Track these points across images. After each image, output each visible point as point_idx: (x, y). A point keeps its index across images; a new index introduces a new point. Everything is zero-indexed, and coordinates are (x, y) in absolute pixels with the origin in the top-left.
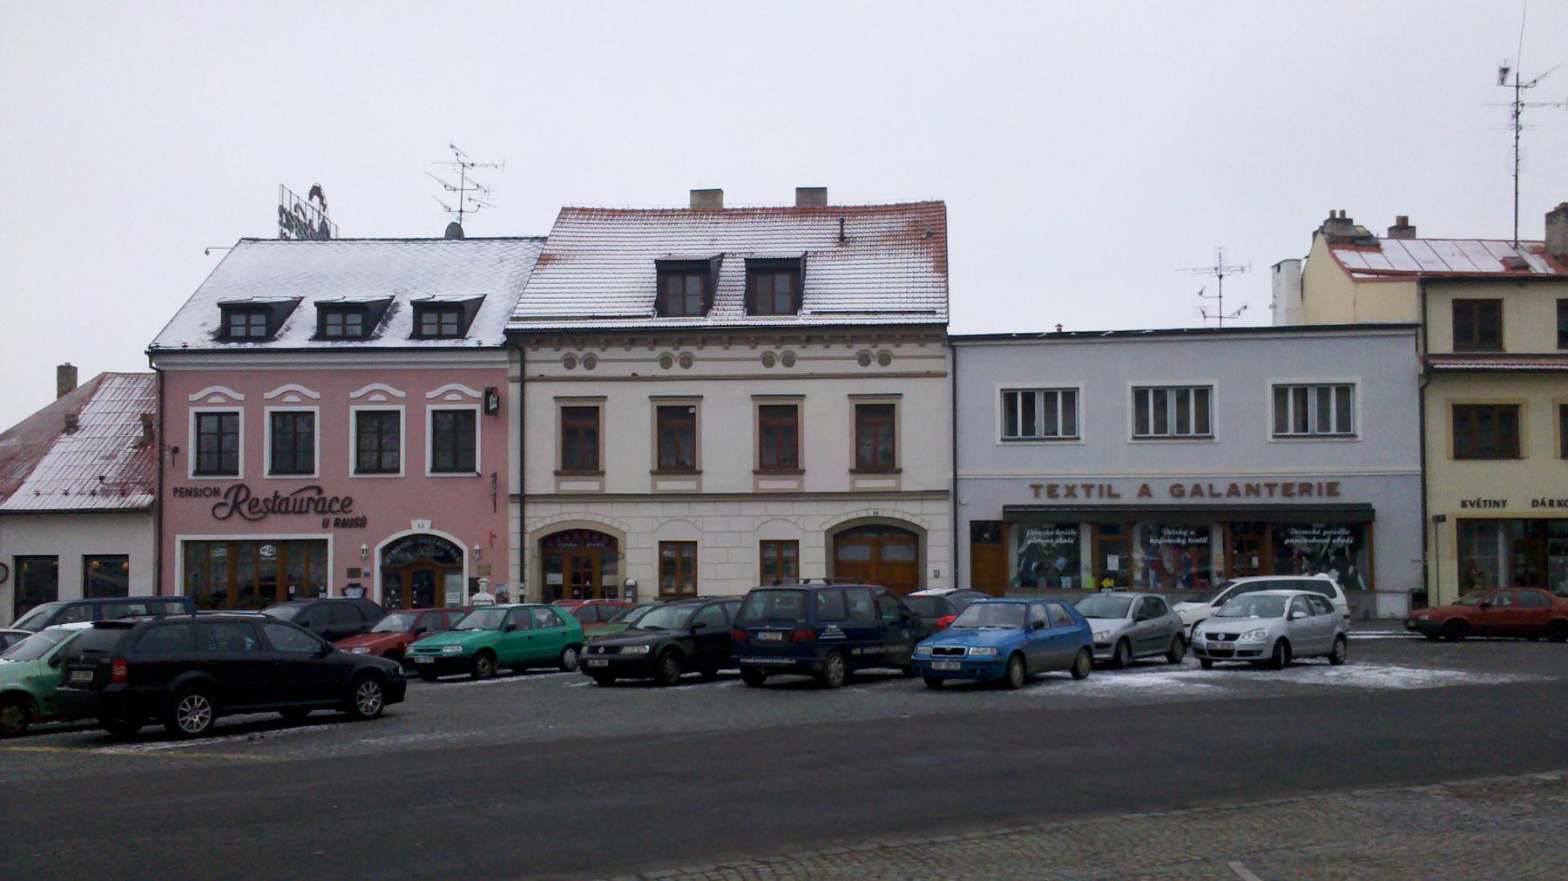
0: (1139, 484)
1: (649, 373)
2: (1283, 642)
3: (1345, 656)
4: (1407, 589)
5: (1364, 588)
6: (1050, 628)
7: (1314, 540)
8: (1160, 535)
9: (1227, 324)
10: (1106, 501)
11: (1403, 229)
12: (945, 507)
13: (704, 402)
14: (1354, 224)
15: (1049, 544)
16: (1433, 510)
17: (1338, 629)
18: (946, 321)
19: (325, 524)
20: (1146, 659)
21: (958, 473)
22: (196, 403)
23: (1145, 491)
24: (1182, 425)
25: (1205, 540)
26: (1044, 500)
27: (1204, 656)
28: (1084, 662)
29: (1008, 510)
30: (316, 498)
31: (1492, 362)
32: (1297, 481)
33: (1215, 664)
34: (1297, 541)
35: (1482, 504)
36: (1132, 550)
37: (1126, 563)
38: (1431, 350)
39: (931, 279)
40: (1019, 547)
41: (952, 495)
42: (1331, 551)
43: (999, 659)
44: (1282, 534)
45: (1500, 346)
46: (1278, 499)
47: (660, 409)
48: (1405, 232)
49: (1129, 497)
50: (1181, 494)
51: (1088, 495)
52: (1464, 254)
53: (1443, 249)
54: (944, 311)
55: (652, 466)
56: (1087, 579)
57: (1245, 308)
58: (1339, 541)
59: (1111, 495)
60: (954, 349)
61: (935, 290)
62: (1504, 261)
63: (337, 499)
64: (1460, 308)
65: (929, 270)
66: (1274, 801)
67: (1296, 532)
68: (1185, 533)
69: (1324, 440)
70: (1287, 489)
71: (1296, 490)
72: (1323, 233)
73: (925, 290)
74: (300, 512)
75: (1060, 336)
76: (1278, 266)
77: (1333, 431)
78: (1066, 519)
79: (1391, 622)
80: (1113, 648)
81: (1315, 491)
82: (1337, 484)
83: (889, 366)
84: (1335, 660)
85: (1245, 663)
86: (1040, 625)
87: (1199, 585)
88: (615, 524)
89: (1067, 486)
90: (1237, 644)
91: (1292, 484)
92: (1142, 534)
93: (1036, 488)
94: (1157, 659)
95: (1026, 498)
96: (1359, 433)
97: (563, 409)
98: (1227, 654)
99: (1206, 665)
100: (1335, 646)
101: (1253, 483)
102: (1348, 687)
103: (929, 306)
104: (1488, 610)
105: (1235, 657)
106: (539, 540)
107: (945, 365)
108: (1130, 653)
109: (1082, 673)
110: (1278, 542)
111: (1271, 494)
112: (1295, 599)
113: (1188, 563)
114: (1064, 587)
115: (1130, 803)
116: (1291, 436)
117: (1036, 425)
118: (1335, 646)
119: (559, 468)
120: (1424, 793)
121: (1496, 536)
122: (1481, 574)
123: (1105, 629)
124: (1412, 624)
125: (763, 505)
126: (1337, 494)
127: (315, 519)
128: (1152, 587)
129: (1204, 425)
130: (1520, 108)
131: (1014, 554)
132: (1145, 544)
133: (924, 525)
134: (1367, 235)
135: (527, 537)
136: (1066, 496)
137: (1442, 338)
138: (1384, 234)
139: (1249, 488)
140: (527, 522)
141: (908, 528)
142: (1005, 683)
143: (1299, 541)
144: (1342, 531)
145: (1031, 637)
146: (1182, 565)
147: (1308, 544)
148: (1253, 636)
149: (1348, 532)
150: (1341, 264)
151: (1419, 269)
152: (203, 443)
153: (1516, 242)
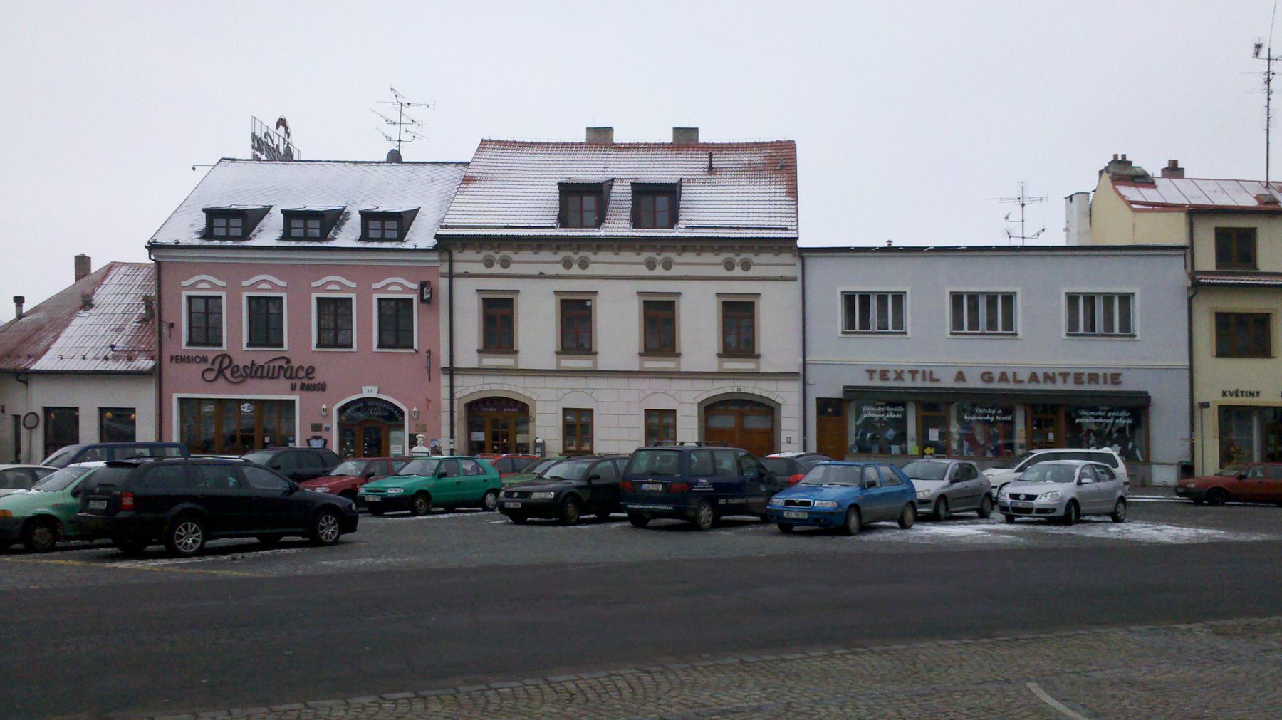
0: (955, 371)
1: (553, 272)
2: (1073, 502)
3: (1125, 515)
5: (1141, 460)
6: (881, 486)
7: (1100, 420)
8: (972, 413)
9: (1028, 243)
10: (928, 384)
11: (1173, 170)
12: (796, 386)
14: (1134, 165)
15: (881, 419)
16: (1200, 397)
17: (1119, 493)
18: (796, 236)
20: (961, 514)
21: (807, 359)
22: (378, 291)
23: (960, 376)
24: (992, 324)
25: (1008, 418)
26: (877, 382)
28: (909, 515)
29: (847, 390)
31: (1247, 278)
33: (1017, 519)
34: (1086, 420)
35: (1240, 394)
36: (949, 425)
37: (944, 435)
40: (856, 420)
41: (802, 376)
42: (1114, 430)
43: (840, 510)
44: (1073, 415)
45: (1254, 266)
46: (1071, 386)
48: (1176, 172)
49: (947, 382)
50: (991, 380)
51: (913, 379)
52: (1224, 191)
53: (1208, 187)
54: (794, 228)
56: (912, 447)
57: (1043, 230)
58: (1121, 421)
59: (933, 380)
60: (803, 258)
61: (787, 211)
62: (1257, 198)
63: (301, 368)
64: (1222, 235)
65: (782, 195)
66: (1065, 633)
67: (1085, 413)
68: (994, 412)
70: (1078, 378)
71: (1085, 378)
72: (1108, 172)
74: (273, 378)
75: (890, 250)
76: (1071, 198)
77: (1117, 331)
78: (895, 398)
79: (1164, 488)
80: (933, 504)
81: (1101, 380)
82: (1119, 375)
84: (1116, 519)
85: (1042, 519)
86: (872, 484)
87: (1005, 454)
88: (527, 394)
89: (896, 371)
90: (1036, 503)
91: (1083, 374)
92: (958, 412)
93: (871, 372)
94: (970, 514)
95: (862, 380)
96: (1138, 333)
98: (1028, 511)
99: (1010, 520)
101: (1050, 372)
104: (1244, 480)
105: (1034, 514)
107: (796, 271)
108: (947, 509)
109: (908, 524)
110: (1070, 421)
111: (1065, 381)
112: (1084, 467)
113: (996, 437)
114: (893, 453)
115: (946, 631)
120: (1189, 630)
121: (1251, 420)
122: (1238, 452)
123: (926, 488)
124: (1181, 490)
127: (284, 383)
130: (1271, 77)
131: (852, 425)
132: (960, 420)
134: (1144, 174)
135: (456, 402)
136: (896, 379)
137: (1206, 259)
138: (1159, 174)
140: (455, 390)
142: (844, 531)
144: (1124, 413)
146: (991, 438)
148: (1048, 497)
150: (1123, 197)
152: (193, 319)
153: (1268, 182)
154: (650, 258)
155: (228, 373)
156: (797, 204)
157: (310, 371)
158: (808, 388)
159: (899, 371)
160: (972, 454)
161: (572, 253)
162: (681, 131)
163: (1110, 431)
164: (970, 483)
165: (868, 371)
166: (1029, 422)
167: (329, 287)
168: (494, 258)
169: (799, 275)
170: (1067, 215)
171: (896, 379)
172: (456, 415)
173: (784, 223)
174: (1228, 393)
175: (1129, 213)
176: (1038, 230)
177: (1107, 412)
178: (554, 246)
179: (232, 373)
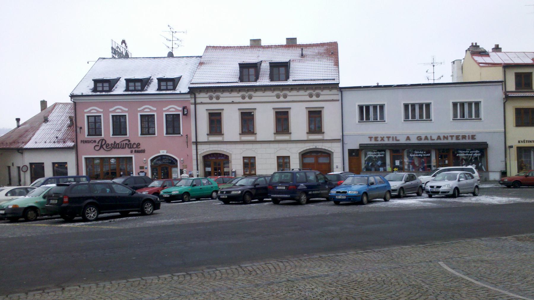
1: (238, 101)
2: (456, 188)
4: (500, 171)
5: (484, 170)
7: (467, 154)
8: (413, 153)
9: (436, 82)
10: (395, 142)
11: (497, 49)
12: (339, 145)
13: (257, 111)
14: (480, 47)
15: (375, 157)
16: (508, 144)
17: (476, 184)
18: (338, 82)
19: (132, 152)
20: (409, 195)
22: (165, 111)
23: (408, 138)
24: (421, 116)
25: (429, 155)
26: (373, 142)
27: (429, 194)
28: (388, 196)
29: (361, 145)
30: (128, 143)
32: (461, 135)
33: (433, 196)
34: (461, 155)
35: (525, 142)
37: (402, 163)
38: (508, 89)
39: (333, 68)
40: (365, 158)
41: (342, 140)
42: (473, 158)
43: (359, 195)
44: (456, 153)
46: (454, 141)
49: (403, 140)
50: (421, 139)
51: (388, 140)
52: (518, 57)
53: (510, 55)
56: (389, 168)
57: (442, 76)
58: (476, 155)
59: (396, 140)
60: (341, 92)
64: (518, 75)
65: (332, 65)
67: (461, 152)
68: (422, 153)
69: (471, 120)
70: (457, 137)
71: (460, 137)
72: (469, 51)
73: (331, 72)
74: (123, 148)
75: (378, 87)
76: (454, 62)
78: (381, 148)
79: (494, 181)
80: (398, 191)
81: (467, 138)
82: (475, 135)
83: (312, 98)
84: (475, 195)
85: (443, 196)
86: (372, 184)
87: (427, 170)
88: (228, 151)
89: (381, 137)
90: (441, 190)
91: (459, 136)
93: (371, 138)
97: (209, 113)
98: (437, 193)
99: (430, 196)
100: (475, 190)
101: (446, 136)
102: (479, 203)
103: (332, 77)
105: (440, 194)
107: (339, 97)
108: (404, 193)
110: (454, 155)
111: (452, 139)
113: (423, 163)
114: (380, 171)
116: (459, 120)
117: (370, 117)
118: (475, 190)
120: (506, 239)
123: (395, 185)
124: (501, 182)
126: (475, 139)
127: (128, 150)
128: (411, 170)
129: (428, 116)
131: (363, 160)
132: (408, 156)
134: (485, 51)
135: (198, 156)
136: (381, 140)
137: (511, 86)
138: (490, 50)
139: (444, 137)
142: (361, 203)
143: (462, 155)
144: (477, 151)
145: (370, 187)
146: (421, 163)
147: (465, 156)
149: (479, 152)
150: (476, 61)
151: (502, 62)
155: (104, 147)
156: (338, 69)
157: (138, 145)
158: (344, 145)
159: (382, 137)
160: (414, 170)
163: (471, 159)
164: (413, 182)
165: (369, 137)
166: (437, 155)
167: (171, 110)
169: (340, 99)
170: (452, 70)
171: (381, 140)
173: (334, 77)
174: (520, 142)
175: (479, 68)
176: (440, 76)
177: (470, 151)
179: (106, 147)
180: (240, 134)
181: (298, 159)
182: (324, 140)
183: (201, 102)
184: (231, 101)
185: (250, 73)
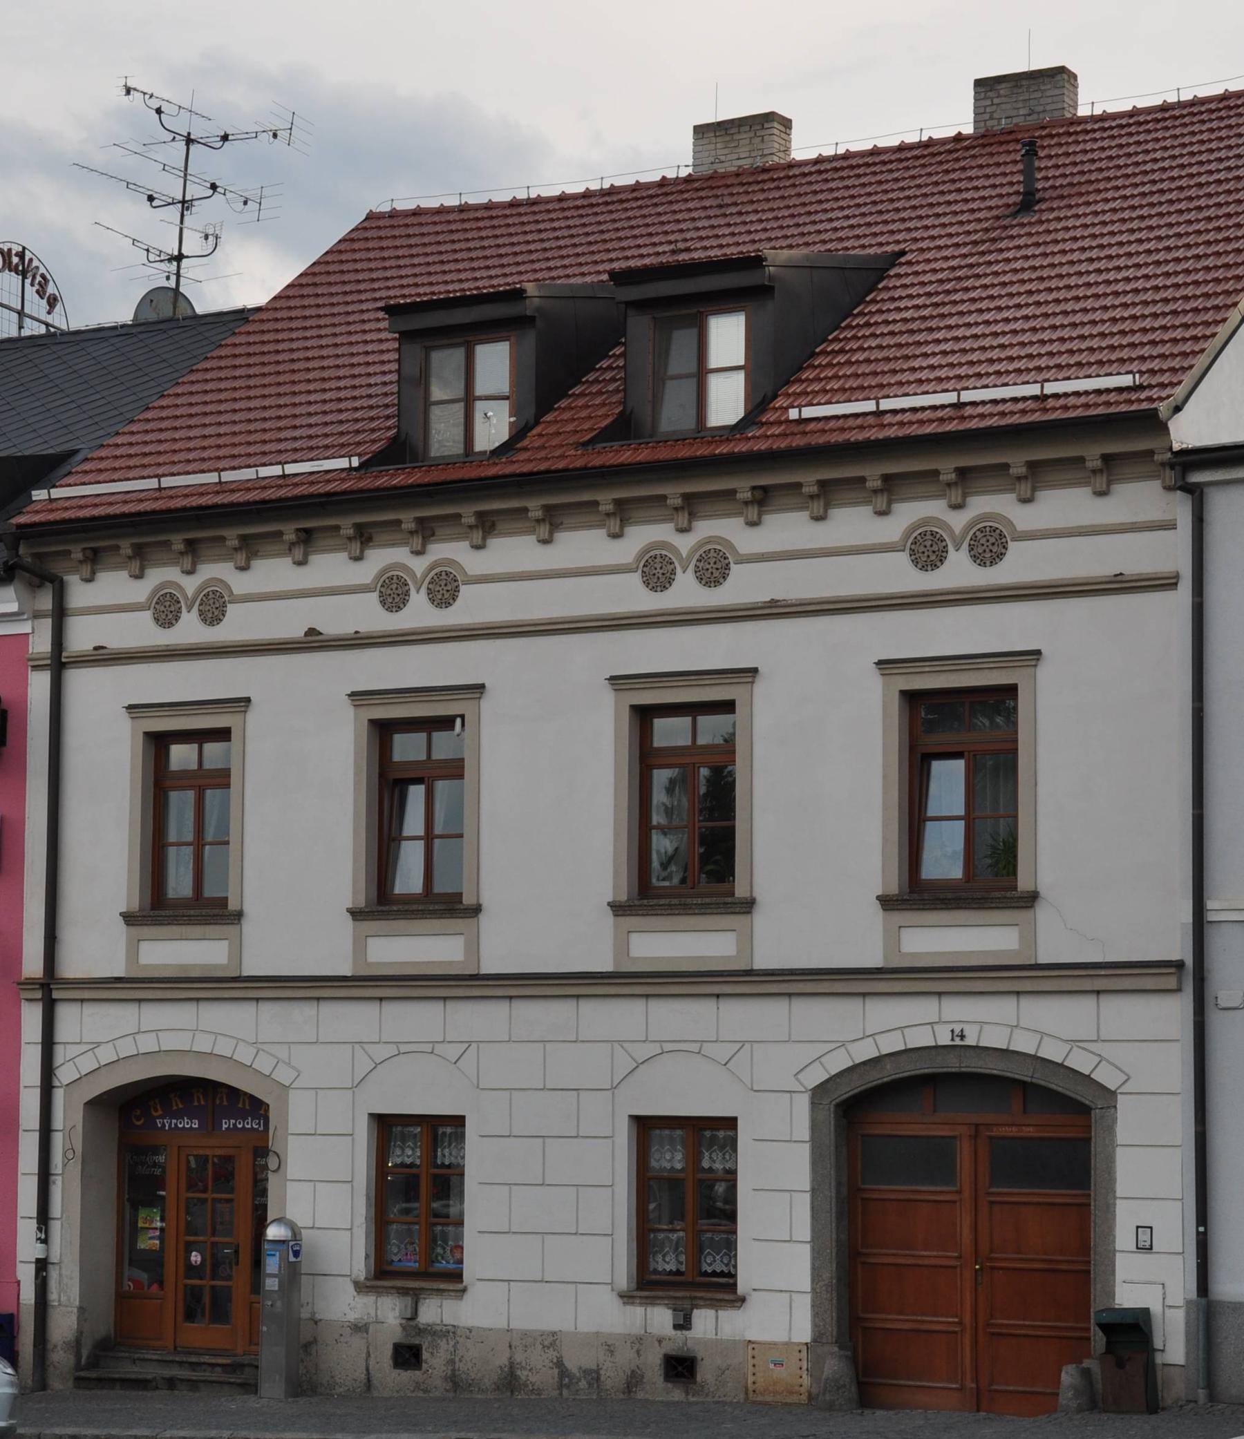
1: (344, 627)
13: (487, 704)
21: (1210, 904)
47: (911, 698)
54: (621, 363)
55: (885, 883)
60: (1197, 494)
83: (720, 589)
88: (264, 1064)
97: (911, 698)
106: (838, 1106)
119: (135, 906)
125: (638, 1006)
133: (1106, 1077)
135: (59, 1096)
140: (60, 1054)
141: (1058, 1084)
154: (925, 521)
158: (1218, 1023)
161: (670, 527)
162: (1003, 88)
168: (676, 551)
169: (1184, 565)
172: (58, 1141)
178: (179, 546)
180: (618, 909)
181: (805, 1152)
182: (749, 972)
183: (357, 632)
184: (298, 633)
185: (482, 386)
